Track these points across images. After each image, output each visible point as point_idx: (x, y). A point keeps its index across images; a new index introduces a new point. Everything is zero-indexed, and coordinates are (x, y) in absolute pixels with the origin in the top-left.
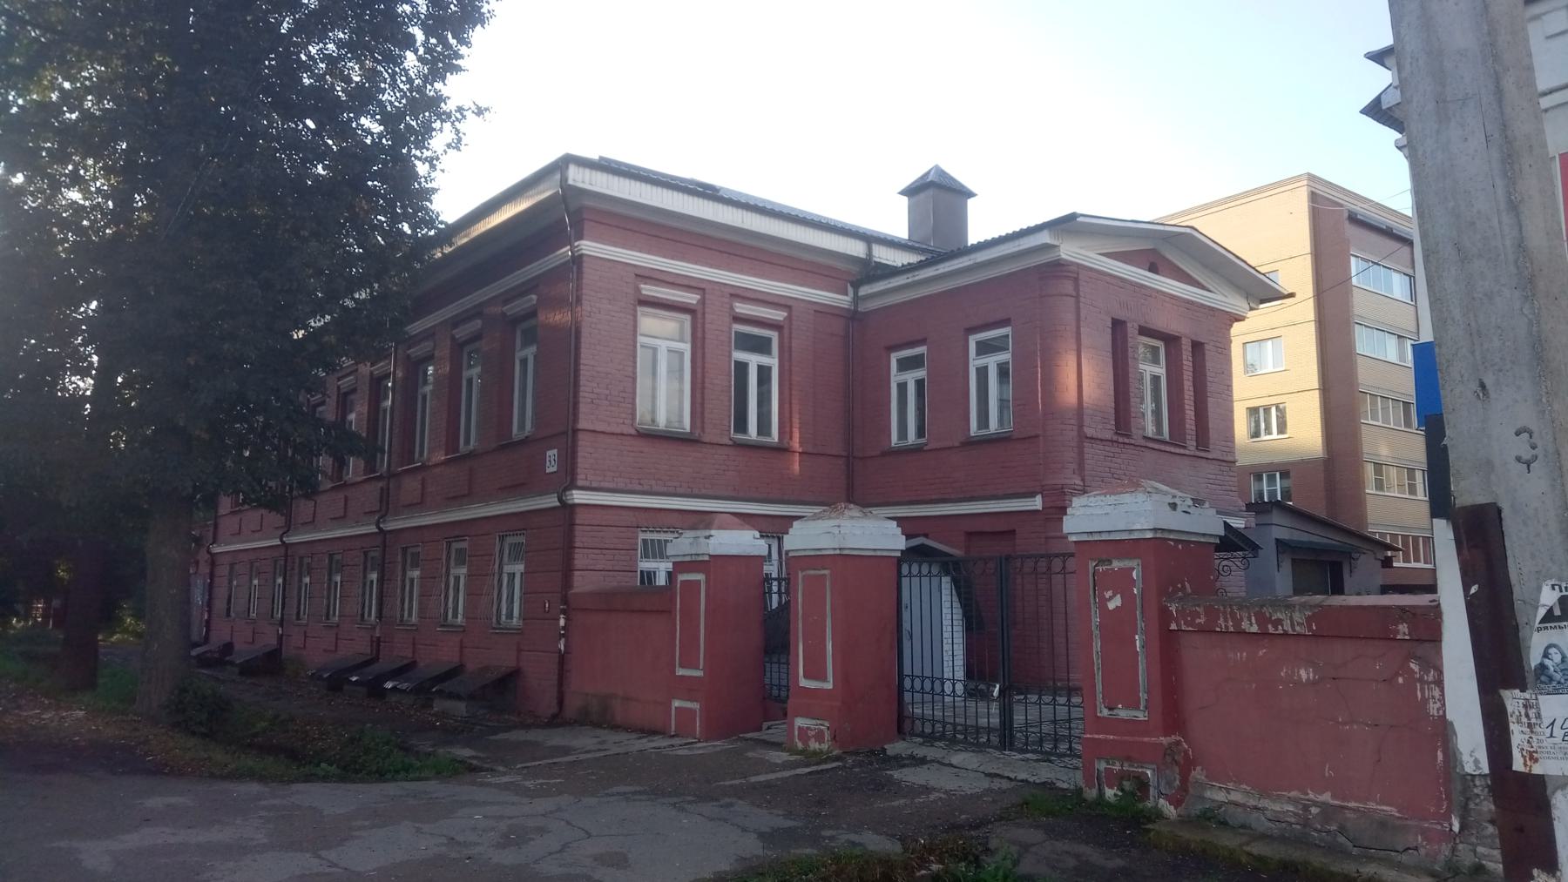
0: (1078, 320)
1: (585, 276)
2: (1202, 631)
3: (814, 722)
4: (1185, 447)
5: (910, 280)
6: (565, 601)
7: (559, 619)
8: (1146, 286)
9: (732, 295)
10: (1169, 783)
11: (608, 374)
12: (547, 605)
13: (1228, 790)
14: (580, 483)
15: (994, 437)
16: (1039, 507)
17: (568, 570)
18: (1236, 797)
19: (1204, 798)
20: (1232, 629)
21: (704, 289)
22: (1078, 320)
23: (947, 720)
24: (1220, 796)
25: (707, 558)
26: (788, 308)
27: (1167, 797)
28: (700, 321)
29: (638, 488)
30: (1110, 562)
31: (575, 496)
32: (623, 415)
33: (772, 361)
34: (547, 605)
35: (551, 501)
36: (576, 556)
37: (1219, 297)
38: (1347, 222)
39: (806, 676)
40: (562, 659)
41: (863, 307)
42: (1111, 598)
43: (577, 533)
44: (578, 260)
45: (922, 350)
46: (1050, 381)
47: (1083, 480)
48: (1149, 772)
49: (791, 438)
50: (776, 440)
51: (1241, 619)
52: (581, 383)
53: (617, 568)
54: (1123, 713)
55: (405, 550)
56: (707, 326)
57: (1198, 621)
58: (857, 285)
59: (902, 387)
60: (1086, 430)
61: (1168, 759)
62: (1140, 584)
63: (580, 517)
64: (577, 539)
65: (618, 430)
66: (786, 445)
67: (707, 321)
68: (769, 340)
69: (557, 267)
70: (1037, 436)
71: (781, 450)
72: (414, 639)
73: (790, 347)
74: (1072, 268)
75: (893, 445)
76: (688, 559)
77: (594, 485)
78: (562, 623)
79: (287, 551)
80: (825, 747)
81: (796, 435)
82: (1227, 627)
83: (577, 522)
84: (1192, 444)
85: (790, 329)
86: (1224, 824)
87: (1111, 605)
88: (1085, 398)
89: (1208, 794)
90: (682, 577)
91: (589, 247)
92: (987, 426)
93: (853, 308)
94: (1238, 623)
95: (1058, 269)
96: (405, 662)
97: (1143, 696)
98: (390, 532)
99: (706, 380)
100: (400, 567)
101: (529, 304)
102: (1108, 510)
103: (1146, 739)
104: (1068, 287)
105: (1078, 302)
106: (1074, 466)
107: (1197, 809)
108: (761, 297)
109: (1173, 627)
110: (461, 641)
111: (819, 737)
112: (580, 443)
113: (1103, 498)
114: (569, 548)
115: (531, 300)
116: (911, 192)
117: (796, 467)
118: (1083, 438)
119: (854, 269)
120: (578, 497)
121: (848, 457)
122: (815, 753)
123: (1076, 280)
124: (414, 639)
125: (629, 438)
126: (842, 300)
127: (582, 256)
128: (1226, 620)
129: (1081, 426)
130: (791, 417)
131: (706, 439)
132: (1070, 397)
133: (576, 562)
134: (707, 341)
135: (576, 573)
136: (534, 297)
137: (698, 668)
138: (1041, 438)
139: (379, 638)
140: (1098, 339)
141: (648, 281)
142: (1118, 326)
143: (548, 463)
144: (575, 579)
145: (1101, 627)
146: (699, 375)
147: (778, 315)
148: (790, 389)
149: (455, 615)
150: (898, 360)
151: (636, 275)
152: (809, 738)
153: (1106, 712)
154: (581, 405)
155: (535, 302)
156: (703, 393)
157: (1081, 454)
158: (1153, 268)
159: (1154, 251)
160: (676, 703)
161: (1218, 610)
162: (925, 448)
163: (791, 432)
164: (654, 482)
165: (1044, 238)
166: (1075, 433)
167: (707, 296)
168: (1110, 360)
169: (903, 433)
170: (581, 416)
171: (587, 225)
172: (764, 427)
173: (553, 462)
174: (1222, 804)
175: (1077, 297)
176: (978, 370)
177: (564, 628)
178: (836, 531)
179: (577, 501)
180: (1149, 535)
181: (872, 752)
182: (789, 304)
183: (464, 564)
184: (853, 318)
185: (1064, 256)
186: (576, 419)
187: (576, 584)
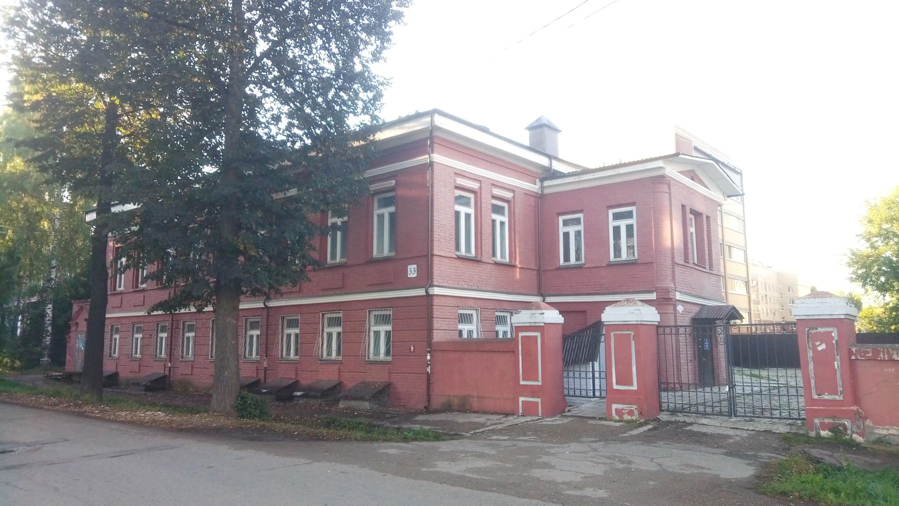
0: (671, 205)
1: (435, 173)
2: (869, 359)
3: (626, 406)
4: (705, 268)
5: (577, 180)
6: (430, 343)
7: (427, 356)
8: (692, 189)
9: (492, 184)
10: (858, 427)
11: (445, 225)
12: (412, 348)
13: (888, 430)
14: (435, 283)
15: (624, 262)
16: (655, 298)
17: (430, 329)
18: (892, 432)
19: (875, 433)
20: (887, 359)
21: (480, 181)
22: (671, 205)
23: (777, 398)
24: (884, 432)
25: (543, 324)
26: (513, 191)
27: (857, 433)
28: (479, 197)
29: (457, 286)
30: (817, 329)
31: (435, 290)
32: (451, 247)
33: (505, 219)
34: (412, 348)
35: (421, 292)
36: (434, 322)
37: (713, 193)
38: (693, 150)
39: (617, 383)
40: (429, 376)
41: (547, 191)
42: (819, 345)
43: (435, 310)
44: (431, 164)
45: (581, 216)
46: (658, 235)
47: (675, 285)
48: (846, 423)
49: (515, 260)
50: (508, 261)
51: (893, 354)
52: (434, 230)
53: (450, 329)
54: (826, 397)
55: (283, 318)
56: (483, 200)
57: (868, 355)
58: (542, 180)
59: (566, 235)
60: (676, 260)
61: (857, 416)
62: (836, 338)
63: (436, 301)
64: (434, 313)
65: (449, 256)
66: (513, 264)
67: (483, 198)
68: (503, 208)
69: (409, 168)
70: (652, 263)
71: (511, 266)
72: (296, 368)
73: (514, 212)
74: (668, 179)
75: (561, 264)
76: (528, 325)
77: (441, 284)
78: (429, 357)
79: (173, 318)
80: (634, 418)
81: (518, 259)
82: (884, 358)
83: (434, 304)
84: (707, 267)
85: (514, 203)
86: (890, 444)
87: (820, 348)
88: (675, 245)
89: (876, 431)
90: (521, 334)
91: (438, 158)
92: (620, 256)
93: (540, 192)
94: (890, 355)
95: (660, 179)
96: (291, 382)
97: (840, 389)
98: (271, 307)
99: (483, 229)
100: (280, 327)
101: (390, 185)
102: (819, 305)
103: (844, 408)
104: (666, 189)
105: (670, 196)
106: (671, 278)
107: (873, 438)
108: (503, 185)
109: (853, 358)
110: (339, 369)
111: (631, 413)
112: (434, 262)
113: (813, 299)
114: (430, 318)
115: (392, 183)
116: (531, 128)
117: (518, 275)
118: (674, 264)
119: (540, 171)
120: (436, 291)
121: (538, 270)
122: (628, 422)
123: (669, 185)
124: (296, 368)
125: (453, 259)
126: (535, 188)
127: (433, 162)
128: (884, 355)
129: (673, 258)
130: (515, 249)
131: (484, 261)
132: (667, 243)
133: (434, 325)
134: (483, 208)
135: (435, 331)
136: (394, 182)
137: (538, 381)
138: (655, 264)
139: (266, 368)
140: (677, 214)
141: (459, 176)
142: (683, 207)
143: (409, 272)
144: (435, 334)
145: (814, 358)
146: (479, 227)
147: (509, 195)
148: (515, 234)
149: (136, 353)
150: (563, 220)
151: (455, 173)
152: (624, 414)
153: (816, 397)
154: (435, 242)
155: (393, 184)
156: (481, 236)
157: (673, 271)
158: (692, 179)
159: (693, 171)
160: (521, 399)
161: (880, 350)
162: (584, 266)
163: (515, 257)
164: (463, 283)
165: (660, 164)
166: (671, 262)
167: (482, 185)
168: (681, 223)
169: (567, 258)
170: (435, 248)
171: (435, 146)
172: (503, 256)
173: (413, 272)
174: (886, 436)
175: (670, 194)
176: (614, 228)
177: (430, 361)
178: (638, 312)
179: (435, 293)
180: (843, 317)
181: (654, 419)
182: (514, 189)
183: (340, 325)
184: (540, 198)
185: (667, 173)
186: (432, 249)
187: (434, 337)
